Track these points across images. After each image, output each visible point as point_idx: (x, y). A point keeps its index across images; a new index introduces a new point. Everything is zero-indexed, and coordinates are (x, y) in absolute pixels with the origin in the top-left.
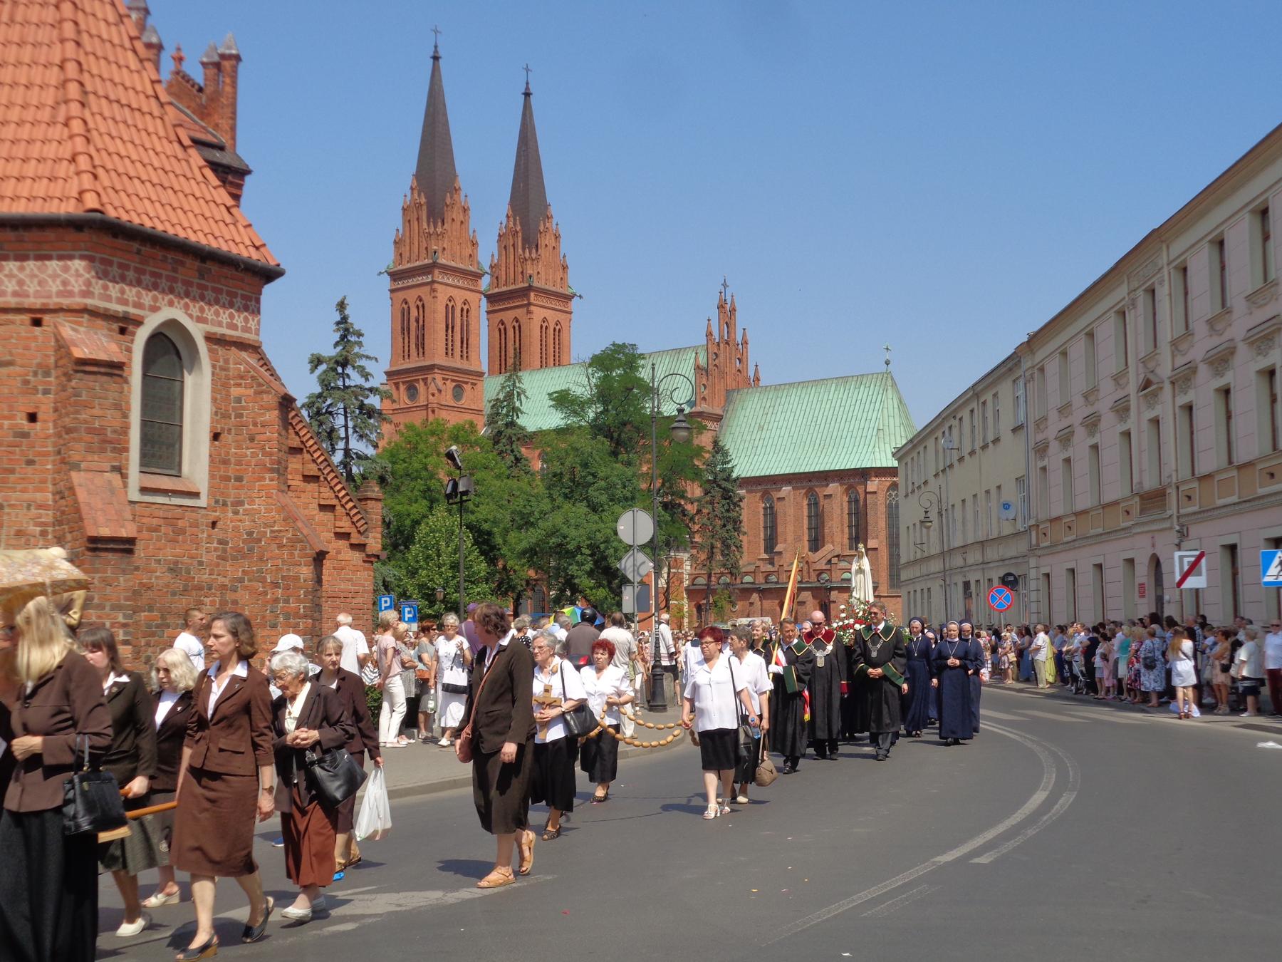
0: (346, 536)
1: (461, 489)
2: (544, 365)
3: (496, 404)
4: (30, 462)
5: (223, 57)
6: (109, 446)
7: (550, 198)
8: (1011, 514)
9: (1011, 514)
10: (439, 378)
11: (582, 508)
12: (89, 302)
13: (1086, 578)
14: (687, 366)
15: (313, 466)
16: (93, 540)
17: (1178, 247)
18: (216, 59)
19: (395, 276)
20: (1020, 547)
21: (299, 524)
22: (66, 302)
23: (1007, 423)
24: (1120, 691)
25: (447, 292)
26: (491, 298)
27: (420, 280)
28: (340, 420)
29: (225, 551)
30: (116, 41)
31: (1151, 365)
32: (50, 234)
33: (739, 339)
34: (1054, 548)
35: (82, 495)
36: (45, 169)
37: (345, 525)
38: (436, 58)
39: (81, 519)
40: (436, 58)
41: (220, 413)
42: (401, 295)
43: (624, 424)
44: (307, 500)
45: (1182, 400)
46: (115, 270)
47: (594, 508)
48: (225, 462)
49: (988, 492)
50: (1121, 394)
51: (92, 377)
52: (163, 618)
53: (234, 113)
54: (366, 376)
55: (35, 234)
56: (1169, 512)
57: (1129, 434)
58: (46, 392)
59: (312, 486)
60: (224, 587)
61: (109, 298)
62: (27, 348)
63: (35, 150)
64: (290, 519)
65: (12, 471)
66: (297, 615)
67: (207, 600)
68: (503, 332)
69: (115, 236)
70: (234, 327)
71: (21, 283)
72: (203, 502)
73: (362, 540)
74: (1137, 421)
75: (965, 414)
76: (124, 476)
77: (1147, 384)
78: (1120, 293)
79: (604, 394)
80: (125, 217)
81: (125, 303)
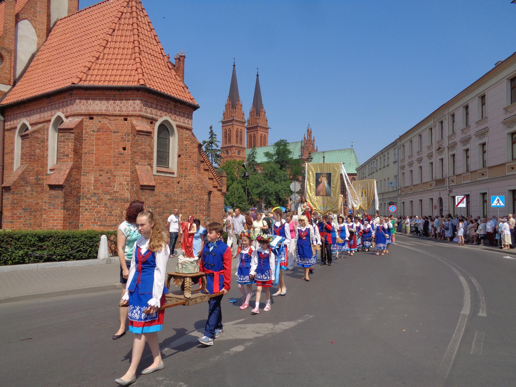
0: (216, 187)
1: (246, 175)
2: (261, 146)
3: (249, 155)
4: (124, 162)
5: (180, 56)
6: (147, 158)
7: (263, 103)
8: (392, 186)
9: (392, 186)
10: (234, 149)
11: (273, 183)
12: (141, 113)
13: (416, 204)
14: (299, 146)
15: (207, 166)
16: (142, 186)
17: (451, 109)
18: (179, 57)
19: (223, 123)
20: (396, 194)
21: (204, 183)
22: (134, 113)
23: (392, 160)
24: (436, 236)
25: (236, 127)
26: (248, 129)
27: (229, 124)
28: (210, 158)
29: (182, 190)
30: (150, 36)
31: (441, 143)
32: (130, 92)
33: (312, 139)
34: (406, 195)
35: (139, 172)
36: (128, 73)
37: (216, 184)
38: (234, 66)
39: (139, 180)
40: (234, 66)
41: (180, 149)
42: (225, 128)
43: (283, 161)
44: (206, 176)
45: (451, 153)
46: (149, 104)
47: (276, 182)
48: (182, 164)
49: (385, 179)
50: (430, 152)
51: (142, 136)
52: (163, 210)
53: (183, 72)
54: (217, 146)
55: (125, 92)
56: (446, 185)
57: (432, 163)
58: (128, 141)
59: (206, 172)
60: (181, 201)
61: (147, 113)
62: (123, 127)
63: (125, 67)
64: (201, 181)
65: (118, 165)
66: (203, 210)
67: (177, 205)
68: (250, 137)
69: (149, 93)
70: (185, 123)
71: (121, 107)
72: (175, 175)
73: (221, 188)
74: (436, 159)
75: (378, 158)
76: (152, 167)
77: (439, 148)
78: (431, 123)
79: (278, 153)
80: (152, 88)
81: (152, 114)
